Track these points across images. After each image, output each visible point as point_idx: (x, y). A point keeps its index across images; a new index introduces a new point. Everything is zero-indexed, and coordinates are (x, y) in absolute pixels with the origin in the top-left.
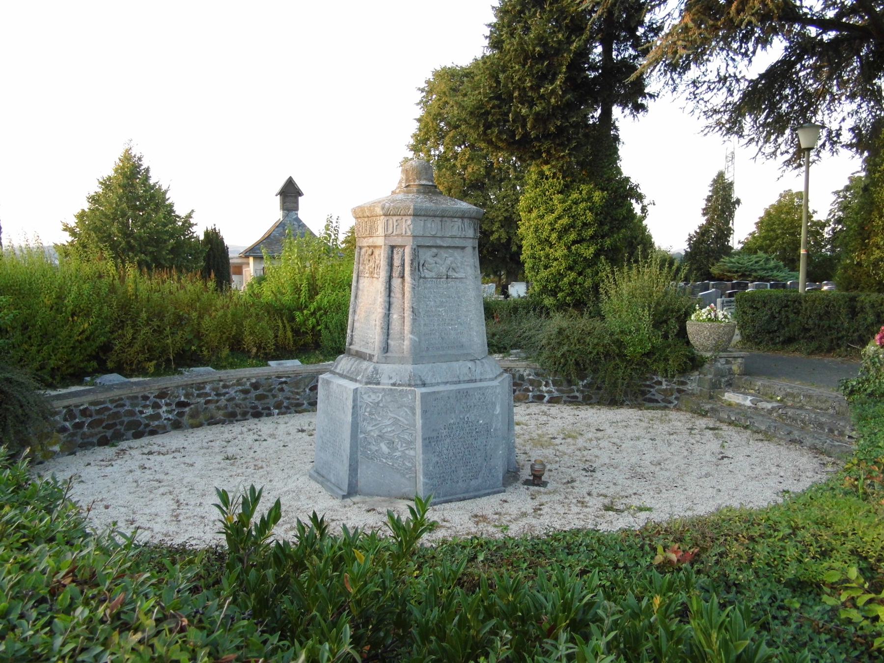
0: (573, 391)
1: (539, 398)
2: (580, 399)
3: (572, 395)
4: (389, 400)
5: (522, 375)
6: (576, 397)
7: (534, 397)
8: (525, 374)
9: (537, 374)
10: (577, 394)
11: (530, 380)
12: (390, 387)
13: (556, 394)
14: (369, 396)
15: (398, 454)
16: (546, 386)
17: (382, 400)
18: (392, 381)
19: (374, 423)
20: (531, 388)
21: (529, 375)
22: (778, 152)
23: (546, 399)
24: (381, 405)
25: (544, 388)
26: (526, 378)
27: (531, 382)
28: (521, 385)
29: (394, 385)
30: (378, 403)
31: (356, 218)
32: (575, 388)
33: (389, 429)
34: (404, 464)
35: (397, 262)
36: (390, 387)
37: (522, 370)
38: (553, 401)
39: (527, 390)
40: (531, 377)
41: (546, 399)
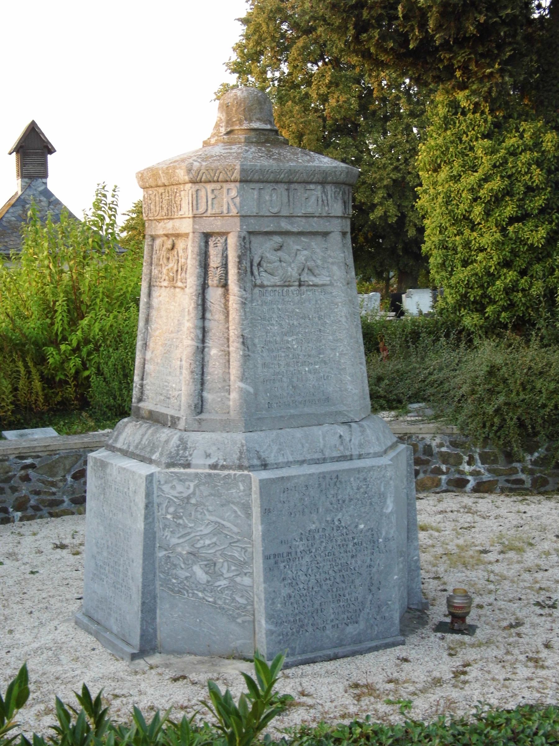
0: (514, 471)
2: (528, 485)
3: (514, 477)
5: (430, 446)
7: (449, 482)
8: (434, 444)
9: (454, 444)
10: (523, 476)
13: (487, 477)
15: (223, 583)
16: (469, 463)
17: (194, 493)
18: (211, 461)
20: (444, 468)
21: (441, 445)
23: (470, 486)
24: (193, 501)
26: (436, 450)
27: (445, 458)
29: (214, 467)
30: (188, 498)
33: (208, 542)
34: (233, 600)
35: (215, 261)
36: (208, 471)
37: (428, 437)
39: (438, 471)
40: (444, 449)
41: (470, 486)
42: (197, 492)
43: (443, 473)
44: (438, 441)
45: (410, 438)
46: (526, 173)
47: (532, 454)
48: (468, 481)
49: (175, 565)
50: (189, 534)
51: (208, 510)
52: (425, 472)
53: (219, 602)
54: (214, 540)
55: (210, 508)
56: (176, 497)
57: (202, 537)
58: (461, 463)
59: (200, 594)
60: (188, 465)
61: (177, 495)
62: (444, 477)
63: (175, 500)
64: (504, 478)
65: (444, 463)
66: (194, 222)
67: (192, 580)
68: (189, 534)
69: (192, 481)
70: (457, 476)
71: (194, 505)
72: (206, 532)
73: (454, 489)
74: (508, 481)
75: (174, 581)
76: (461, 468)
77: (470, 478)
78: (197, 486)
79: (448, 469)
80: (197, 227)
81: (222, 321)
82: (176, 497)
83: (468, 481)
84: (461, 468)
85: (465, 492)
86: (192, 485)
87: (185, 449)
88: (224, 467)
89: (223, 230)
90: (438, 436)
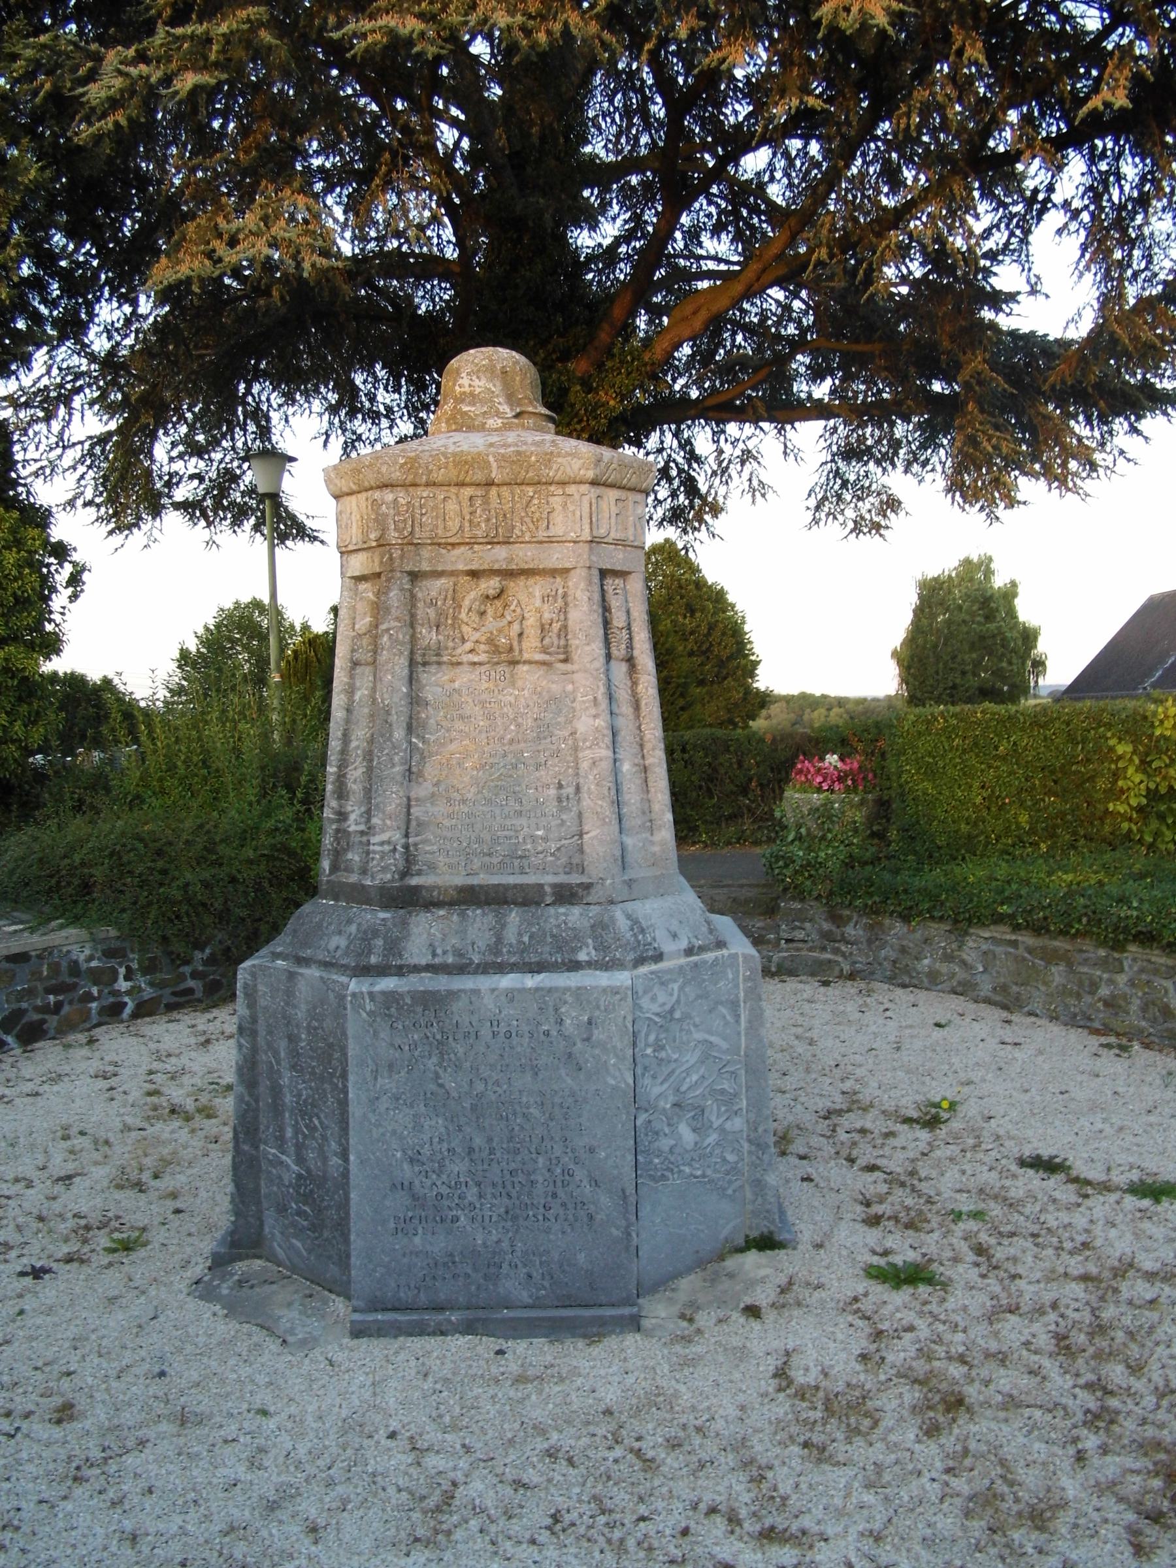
0: (182, 978)
1: (113, 1012)
2: (199, 994)
3: (182, 986)
4: (692, 996)
5: (76, 962)
6: (190, 991)
7: (102, 1011)
8: (82, 957)
9: (109, 954)
10: (191, 983)
11: (90, 969)
12: (683, 961)
13: (148, 993)
14: (654, 999)
15: (713, 1138)
16: (127, 978)
17: (678, 1001)
18: (684, 944)
19: (666, 1070)
20: (95, 991)
21: (90, 958)
22: (80, 502)
23: (128, 1010)
24: (677, 1015)
25: (123, 985)
26: (84, 966)
27: (96, 976)
28: (74, 987)
29: (689, 952)
30: (672, 1011)
31: (337, 497)
32: (187, 969)
33: (695, 1078)
34: (724, 1160)
35: (618, 620)
36: (683, 961)
37: (75, 948)
38: (144, 1010)
39: (88, 997)
40: (94, 964)
41: (128, 1010)
42: (683, 998)
43: (94, 999)
44: (87, 952)
45: (50, 954)
46: (16, 579)
47: (203, 950)
48: (126, 1004)
49: (657, 1133)
50: (673, 1072)
51: (696, 1026)
52: (71, 1003)
53: (709, 1172)
54: (702, 1070)
55: (697, 1020)
56: (657, 1014)
57: (688, 1072)
58: (115, 980)
59: (687, 1170)
60: (659, 957)
61: (659, 1010)
62: (94, 1005)
63: (657, 1019)
64: (168, 991)
65: (95, 984)
66: (591, 549)
67: (677, 1150)
68: (673, 1072)
69: (675, 981)
70: (112, 1000)
71: (679, 1020)
72: (692, 1062)
73: (107, 1019)
74: (174, 994)
75: (656, 1161)
76: (116, 986)
77: (126, 999)
78: (681, 989)
79: (100, 992)
80: (594, 558)
81: (631, 717)
82: (657, 1014)
83: (126, 1004)
84: (116, 986)
85: (122, 1021)
86: (676, 986)
87: (643, 931)
88: (702, 949)
89: (625, 569)
90: (87, 945)
